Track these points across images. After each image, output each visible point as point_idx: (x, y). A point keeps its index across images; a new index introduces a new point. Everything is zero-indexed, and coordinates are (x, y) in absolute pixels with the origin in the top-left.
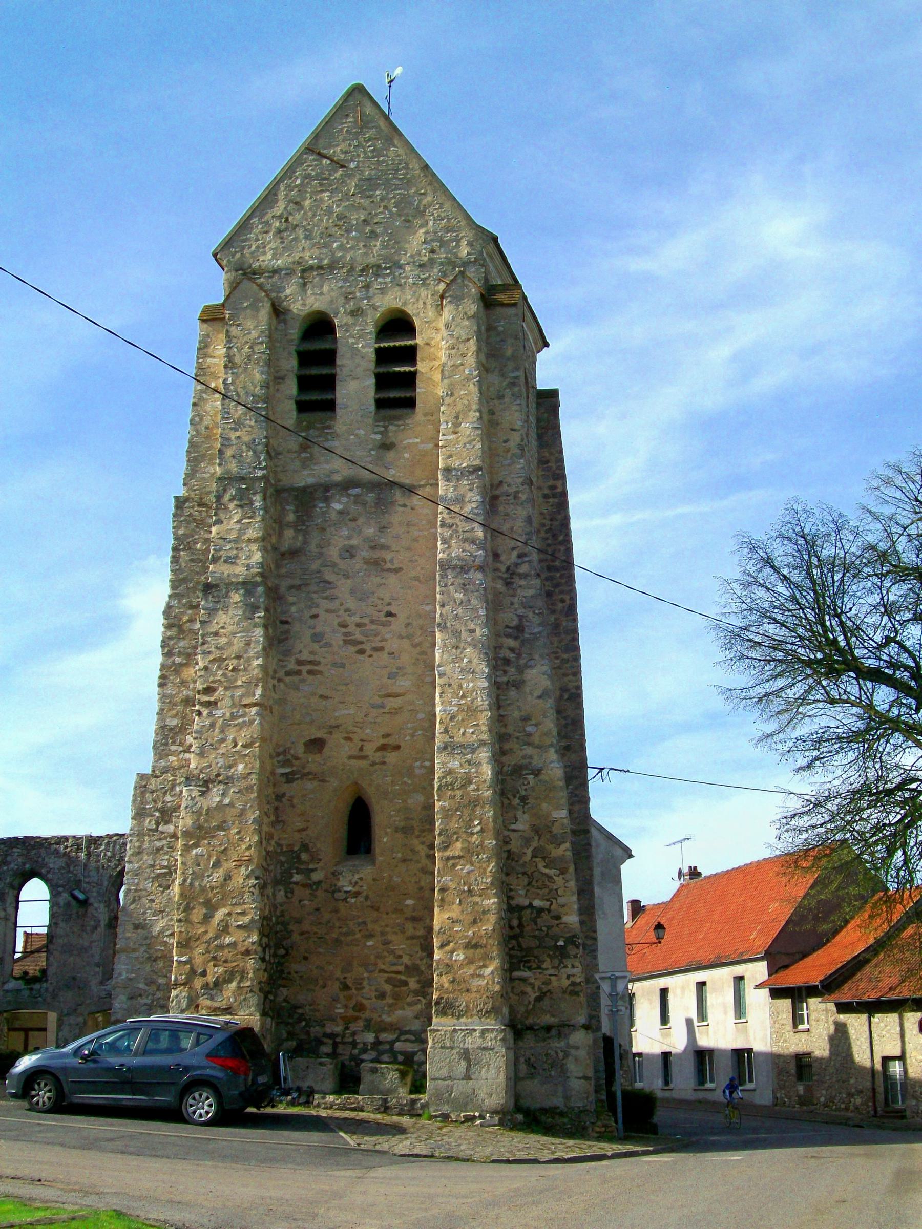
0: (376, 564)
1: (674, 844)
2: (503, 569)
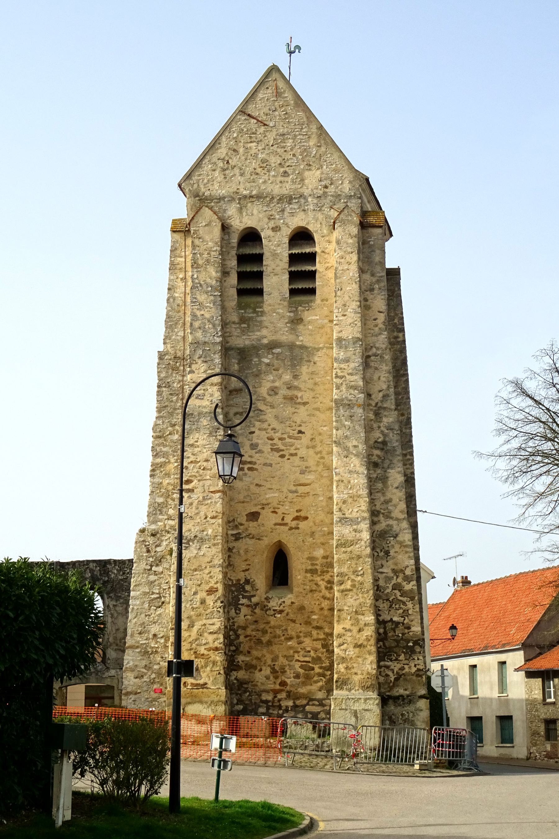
1: (450, 558)
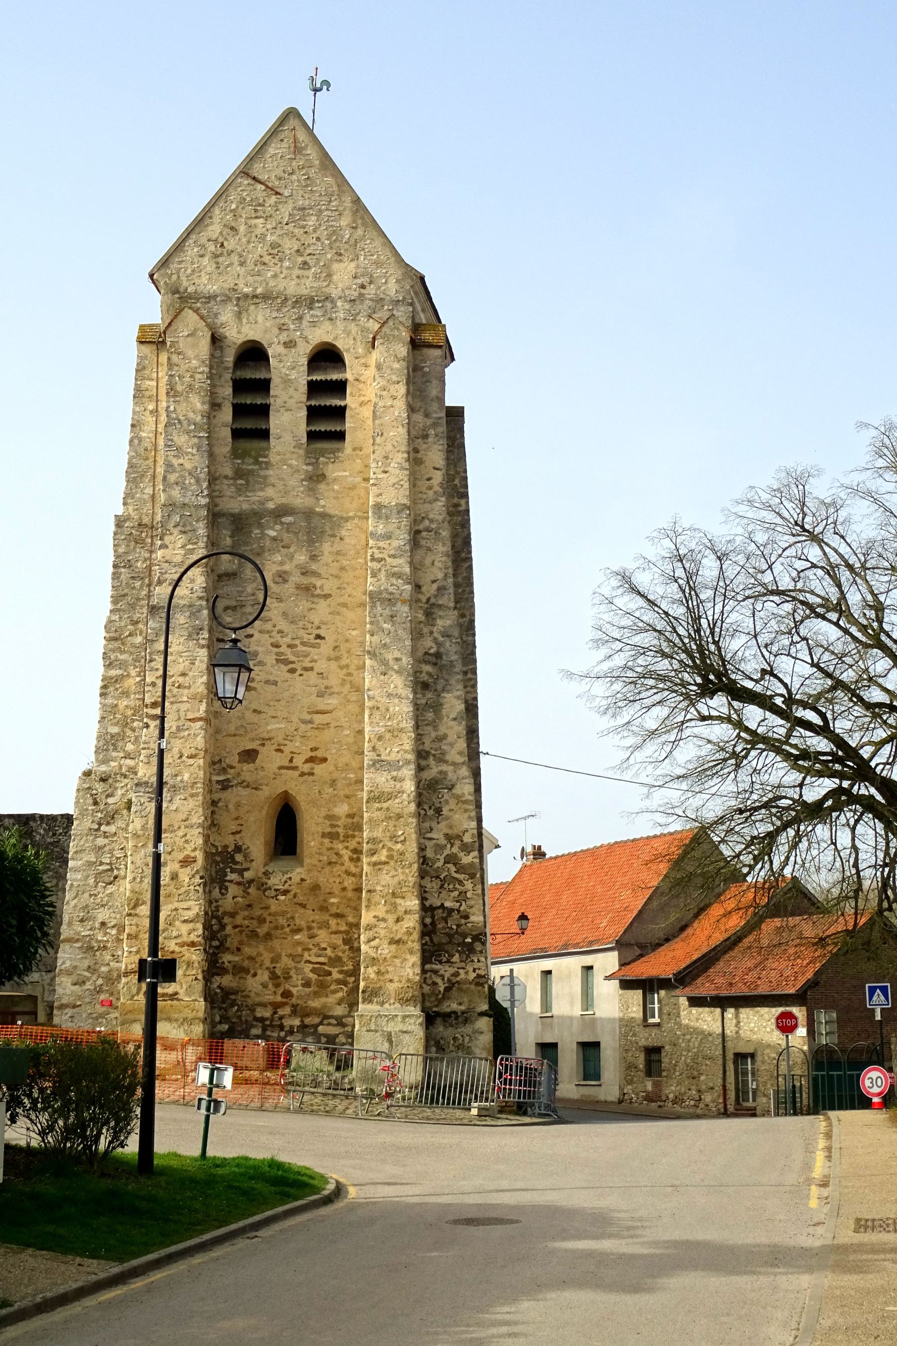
0: (307, 590)
1: (517, 820)
2: (424, 600)
